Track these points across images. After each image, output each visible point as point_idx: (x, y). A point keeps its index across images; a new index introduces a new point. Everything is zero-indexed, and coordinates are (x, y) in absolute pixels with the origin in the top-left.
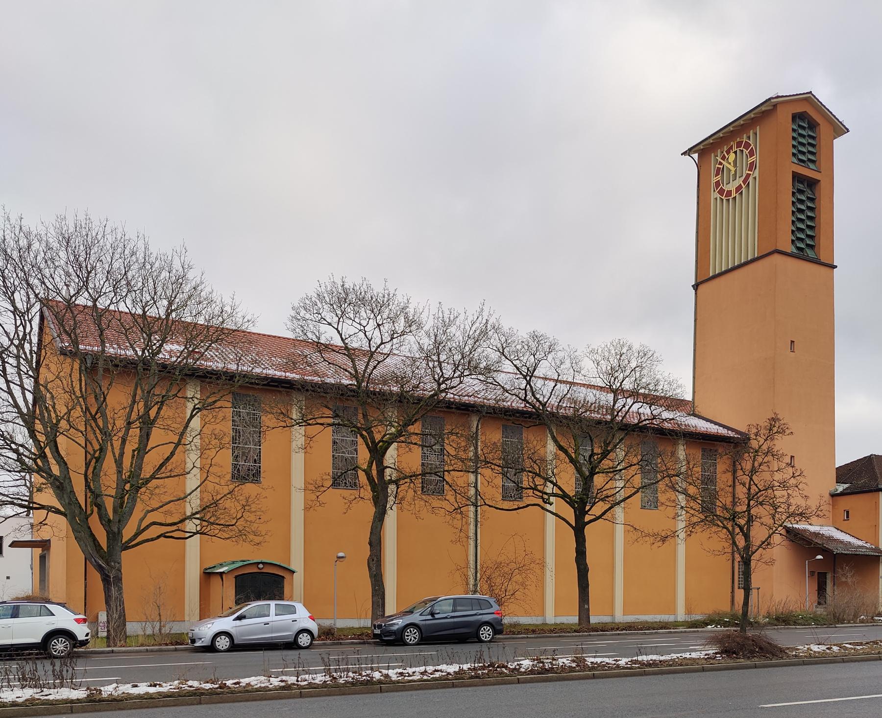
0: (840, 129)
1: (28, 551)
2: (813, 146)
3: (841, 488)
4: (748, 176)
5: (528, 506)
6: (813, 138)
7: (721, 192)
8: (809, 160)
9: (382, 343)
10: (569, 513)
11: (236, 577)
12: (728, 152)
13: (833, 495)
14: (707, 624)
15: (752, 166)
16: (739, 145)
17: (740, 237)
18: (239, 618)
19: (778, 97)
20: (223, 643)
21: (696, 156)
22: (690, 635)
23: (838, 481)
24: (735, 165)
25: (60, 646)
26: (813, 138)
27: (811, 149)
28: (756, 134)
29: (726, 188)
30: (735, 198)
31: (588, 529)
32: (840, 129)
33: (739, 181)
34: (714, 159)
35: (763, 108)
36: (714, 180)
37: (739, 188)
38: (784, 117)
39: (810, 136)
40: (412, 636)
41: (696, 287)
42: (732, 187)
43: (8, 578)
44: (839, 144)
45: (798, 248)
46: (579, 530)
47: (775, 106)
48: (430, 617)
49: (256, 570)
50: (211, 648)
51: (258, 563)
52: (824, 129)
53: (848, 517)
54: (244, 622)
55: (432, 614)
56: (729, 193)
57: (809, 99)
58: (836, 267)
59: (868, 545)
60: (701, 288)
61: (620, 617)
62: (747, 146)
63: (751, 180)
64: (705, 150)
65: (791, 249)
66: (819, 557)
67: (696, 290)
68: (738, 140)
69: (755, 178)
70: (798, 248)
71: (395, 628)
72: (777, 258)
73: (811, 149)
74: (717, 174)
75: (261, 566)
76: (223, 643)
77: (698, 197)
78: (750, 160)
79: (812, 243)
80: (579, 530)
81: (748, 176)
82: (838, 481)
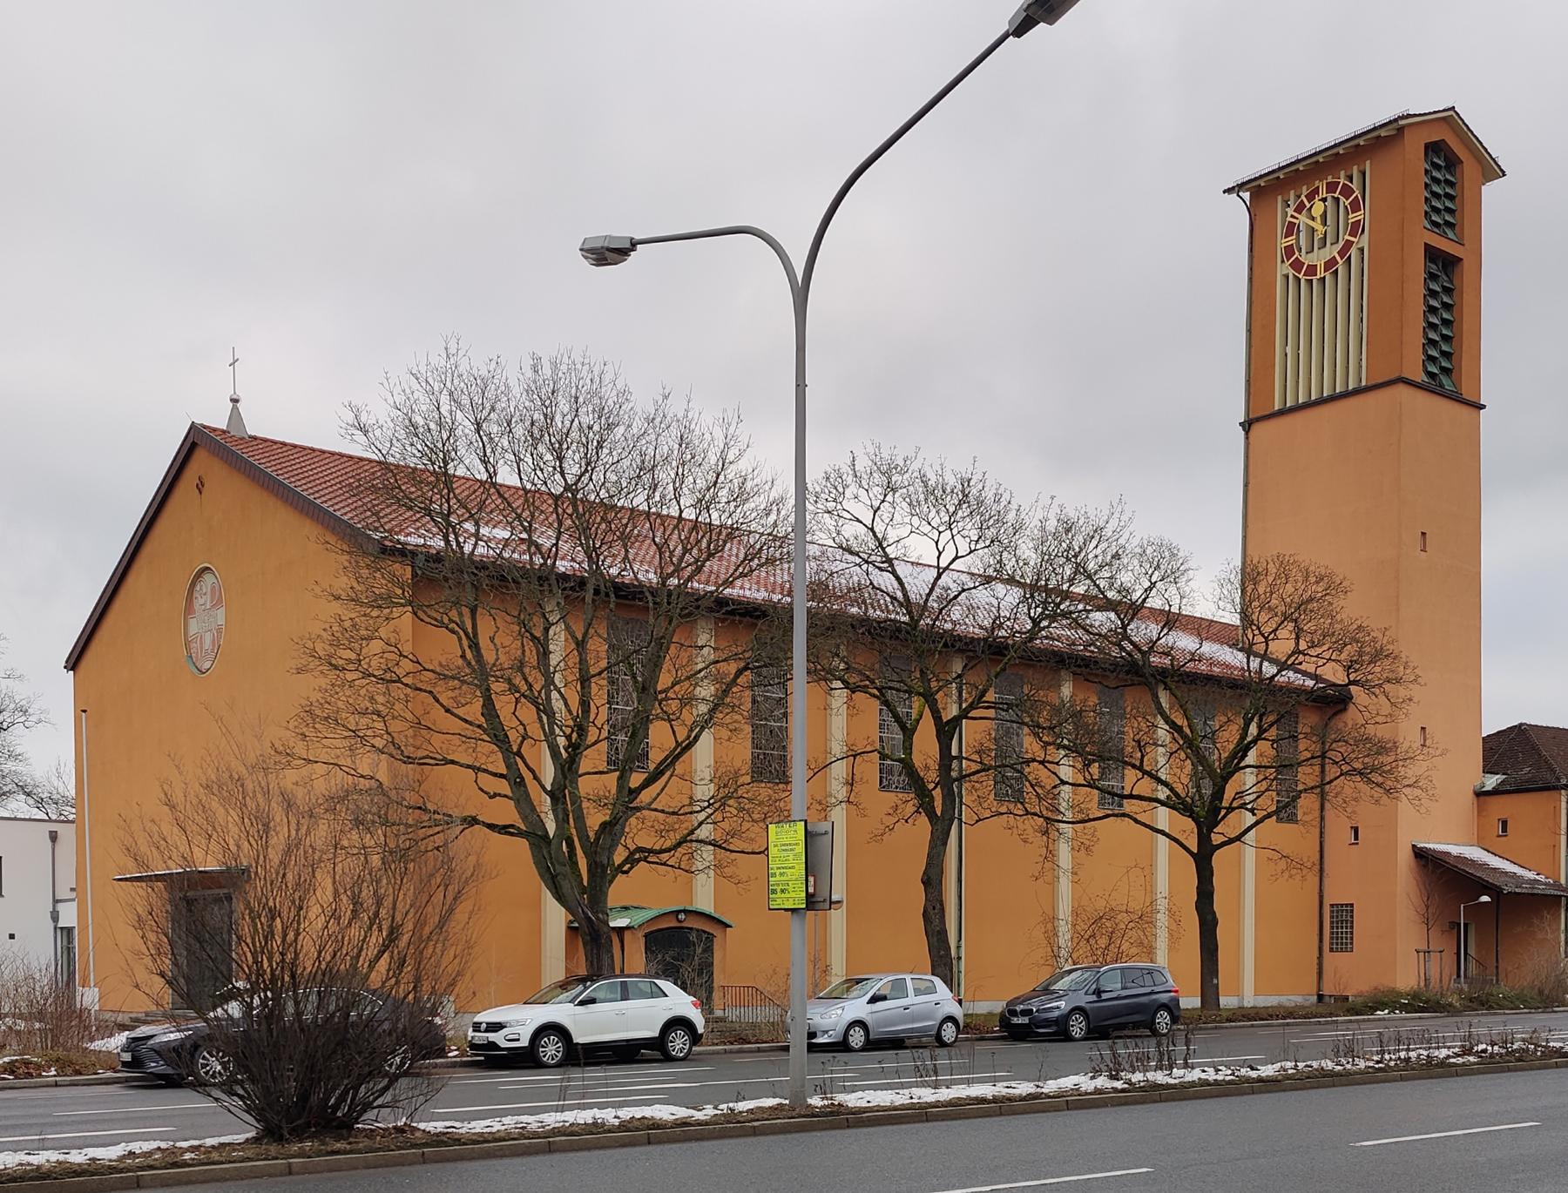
0: (1492, 170)
2: (1451, 198)
3: (1492, 781)
4: (1348, 244)
5: (1124, 815)
6: (1451, 184)
7: (1297, 265)
8: (1448, 224)
9: (957, 557)
10: (1187, 829)
11: (646, 936)
12: (1310, 197)
13: (1480, 794)
14: (1373, 1010)
15: (1356, 229)
16: (1331, 187)
17: (1334, 347)
18: (874, 1000)
19: (1409, 116)
20: (857, 1038)
21: (1246, 195)
22: (1261, 1032)
23: (1488, 770)
24: (1324, 223)
25: (678, 1043)
26: (1451, 184)
27: (1449, 204)
28: (1364, 174)
29: (1307, 260)
31: (1217, 859)
32: (1492, 170)
33: (1332, 251)
34: (1283, 211)
35: (1383, 133)
36: (1283, 243)
37: (1331, 263)
38: (1413, 147)
39: (1447, 182)
40: (1077, 1028)
41: (1247, 425)
42: (1319, 258)
43: (12, 936)
44: (1491, 193)
45: (1431, 375)
46: (1203, 859)
47: (1401, 129)
48: (1094, 998)
49: (674, 924)
50: (842, 1046)
51: (679, 912)
52: (1469, 168)
53: (1505, 830)
54: (880, 1005)
55: (1099, 995)
56: (1312, 270)
57: (1449, 119)
58: (1484, 407)
59: (1541, 878)
60: (1256, 428)
61: (1250, 1000)
62: (1347, 191)
63: (1353, 252)
64: (1263, 191)
65: (1421, 377)
66: (1485, 898)
67: (1247, 433)
68: (1330, 179)
69: (1362, 250)
70: (1431, 375)
71: (1056, 1013)
72: (1402, 389)
73: (1449, 204)
75: (682, 916)
76: (857, 1038)
78: (1353, 217)
79: (1447, 365)
80: (1203, 859)
81: (1348, 244)
82: (1488, 770)
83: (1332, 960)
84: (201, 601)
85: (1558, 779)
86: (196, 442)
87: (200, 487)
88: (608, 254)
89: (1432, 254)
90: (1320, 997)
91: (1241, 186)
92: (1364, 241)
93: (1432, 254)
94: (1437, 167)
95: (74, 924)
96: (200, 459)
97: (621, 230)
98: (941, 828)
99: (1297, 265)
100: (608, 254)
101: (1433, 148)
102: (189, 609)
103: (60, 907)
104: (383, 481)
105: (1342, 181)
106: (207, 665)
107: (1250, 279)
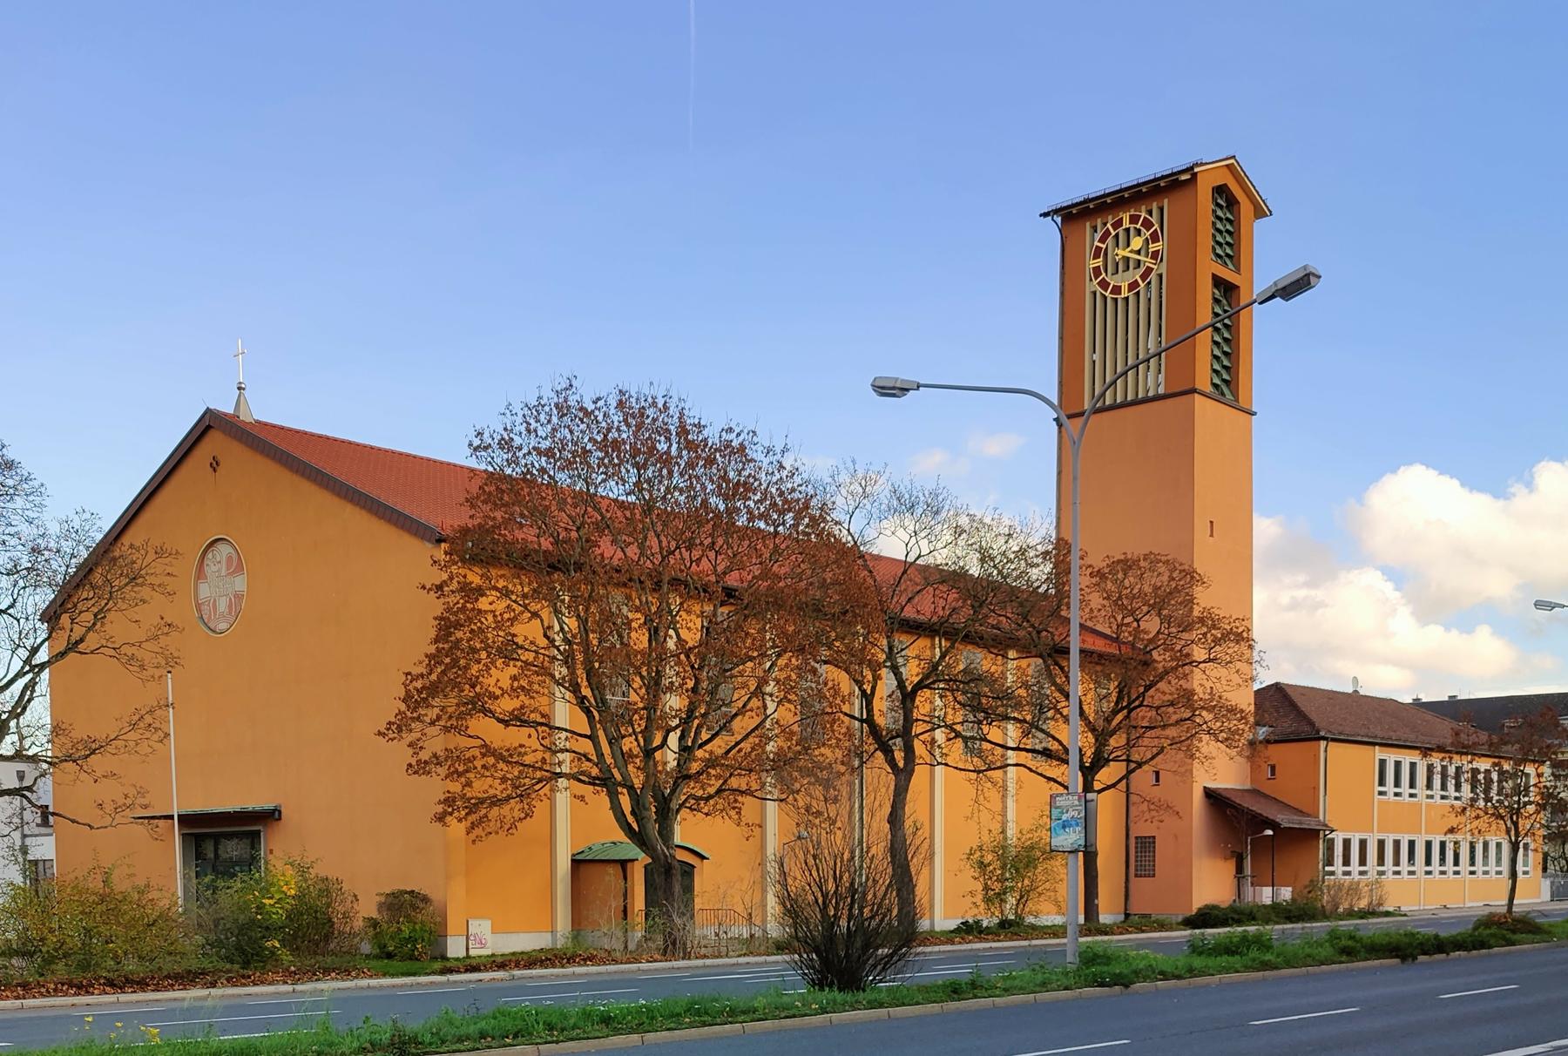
0: (1260, 212)
1: (1505, 902)
3: (1262, 732)
4: (1149, 270)
7: (1104, 284)
16: (1134, 219)
21: (1059, 220)
30: (1127, 299)
32: (1260, 212)
34: (1090, 237)
45: (1215, 386)
52: (1245, 207)
53: (1273, 773)
56: (1117, 290)
62: (1147, 224)
63: (1153, 276)
64: (1073, 216)
66: (1270, 832)
69: (1160, 276)
74: (1096, 256)
77: (1062, 284)
81: (1149, 270)
83: (1137, 884)
84: (214, 568)
85: (1318, 732)
86: (209, 425)
87: (215, 465)
88: (889, 389)
89: (1218, 282)
90: (1127, 916)
91: (1056, 212)
92: (1163, 269)
93: (1218, 282)
94: (1221, 207)
95: (53, 857)
96: (214, 443)
97: (906, 375)
98: (903, 775)
99: (1104, 284)
100: (889, 389)
101: (1221, 190)
102: (200, 573)
103: (28, 841)
104: (497, 489)
105: (1143, 215)
106: (223, 626)
107: (1062, 293)
